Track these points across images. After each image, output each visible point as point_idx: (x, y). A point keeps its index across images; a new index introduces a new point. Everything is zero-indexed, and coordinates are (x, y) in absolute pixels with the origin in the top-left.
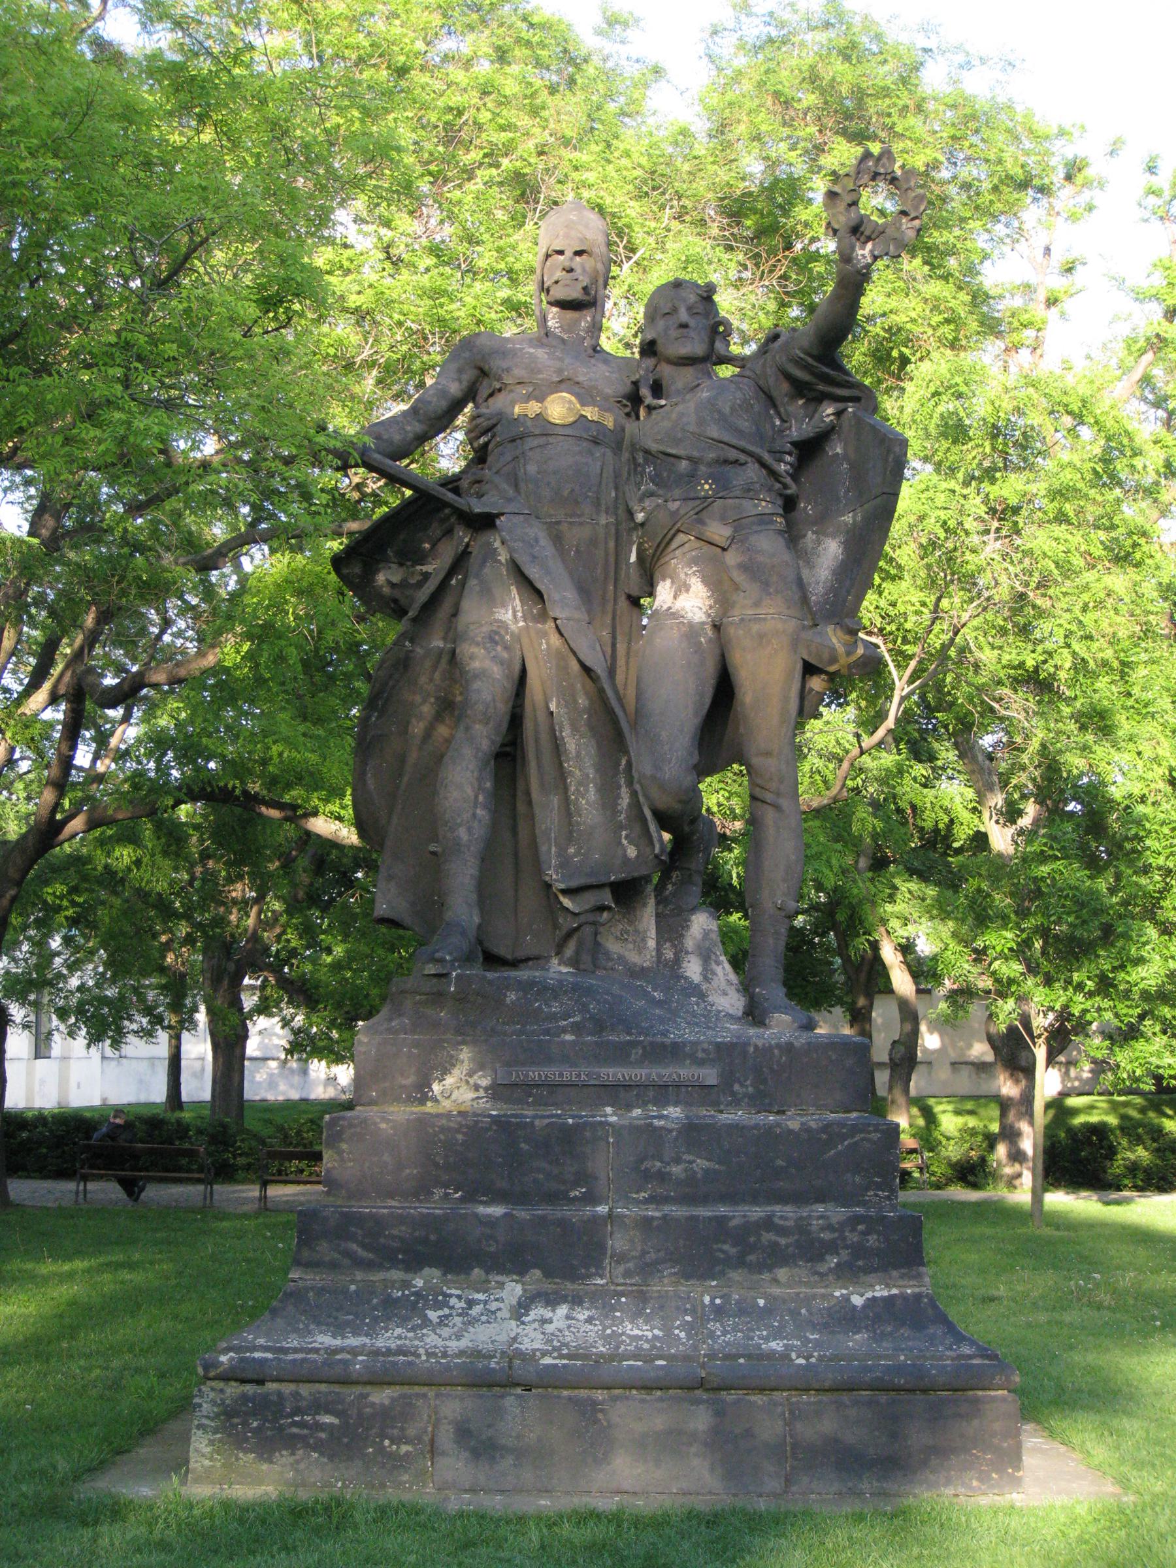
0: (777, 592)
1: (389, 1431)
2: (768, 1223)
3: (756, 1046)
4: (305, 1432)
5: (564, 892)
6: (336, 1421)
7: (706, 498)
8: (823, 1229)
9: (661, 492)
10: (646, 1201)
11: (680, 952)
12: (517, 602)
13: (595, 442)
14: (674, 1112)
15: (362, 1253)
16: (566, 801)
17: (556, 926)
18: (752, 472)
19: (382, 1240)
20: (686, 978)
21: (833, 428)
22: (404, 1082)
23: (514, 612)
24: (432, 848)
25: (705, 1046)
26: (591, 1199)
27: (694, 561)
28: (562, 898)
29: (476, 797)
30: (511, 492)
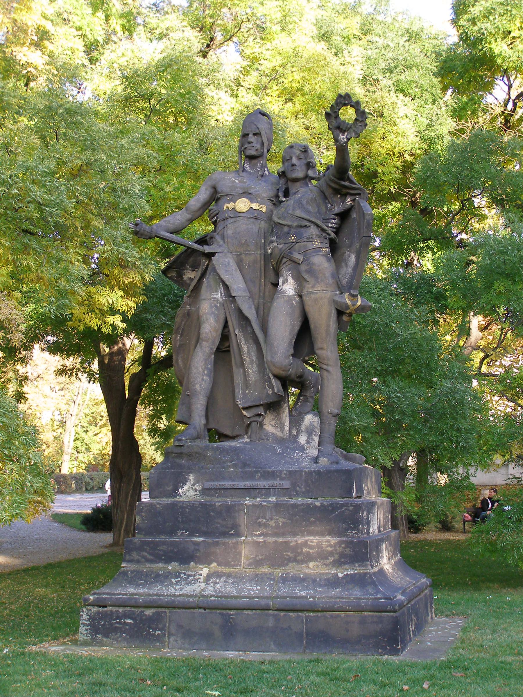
0: (322, 281)
1: (152, 626)
2: (305, 544)
3: (305, 472)
4: (121, 626)
5: (244, 409)
6: (132, 622)
8: (327, 546)
10: (259, 535)
13: (256, 218)
15: (148, 556)
16: (244, 371)
17: (244, 422)
18: (313, 230)
19: (157, 551)
21: (352, 206)
23: (221, 294)
24: (187, 393)
25: (285, 472)
27: (290, 269)
29: (204, 372)
30: (221, 242)
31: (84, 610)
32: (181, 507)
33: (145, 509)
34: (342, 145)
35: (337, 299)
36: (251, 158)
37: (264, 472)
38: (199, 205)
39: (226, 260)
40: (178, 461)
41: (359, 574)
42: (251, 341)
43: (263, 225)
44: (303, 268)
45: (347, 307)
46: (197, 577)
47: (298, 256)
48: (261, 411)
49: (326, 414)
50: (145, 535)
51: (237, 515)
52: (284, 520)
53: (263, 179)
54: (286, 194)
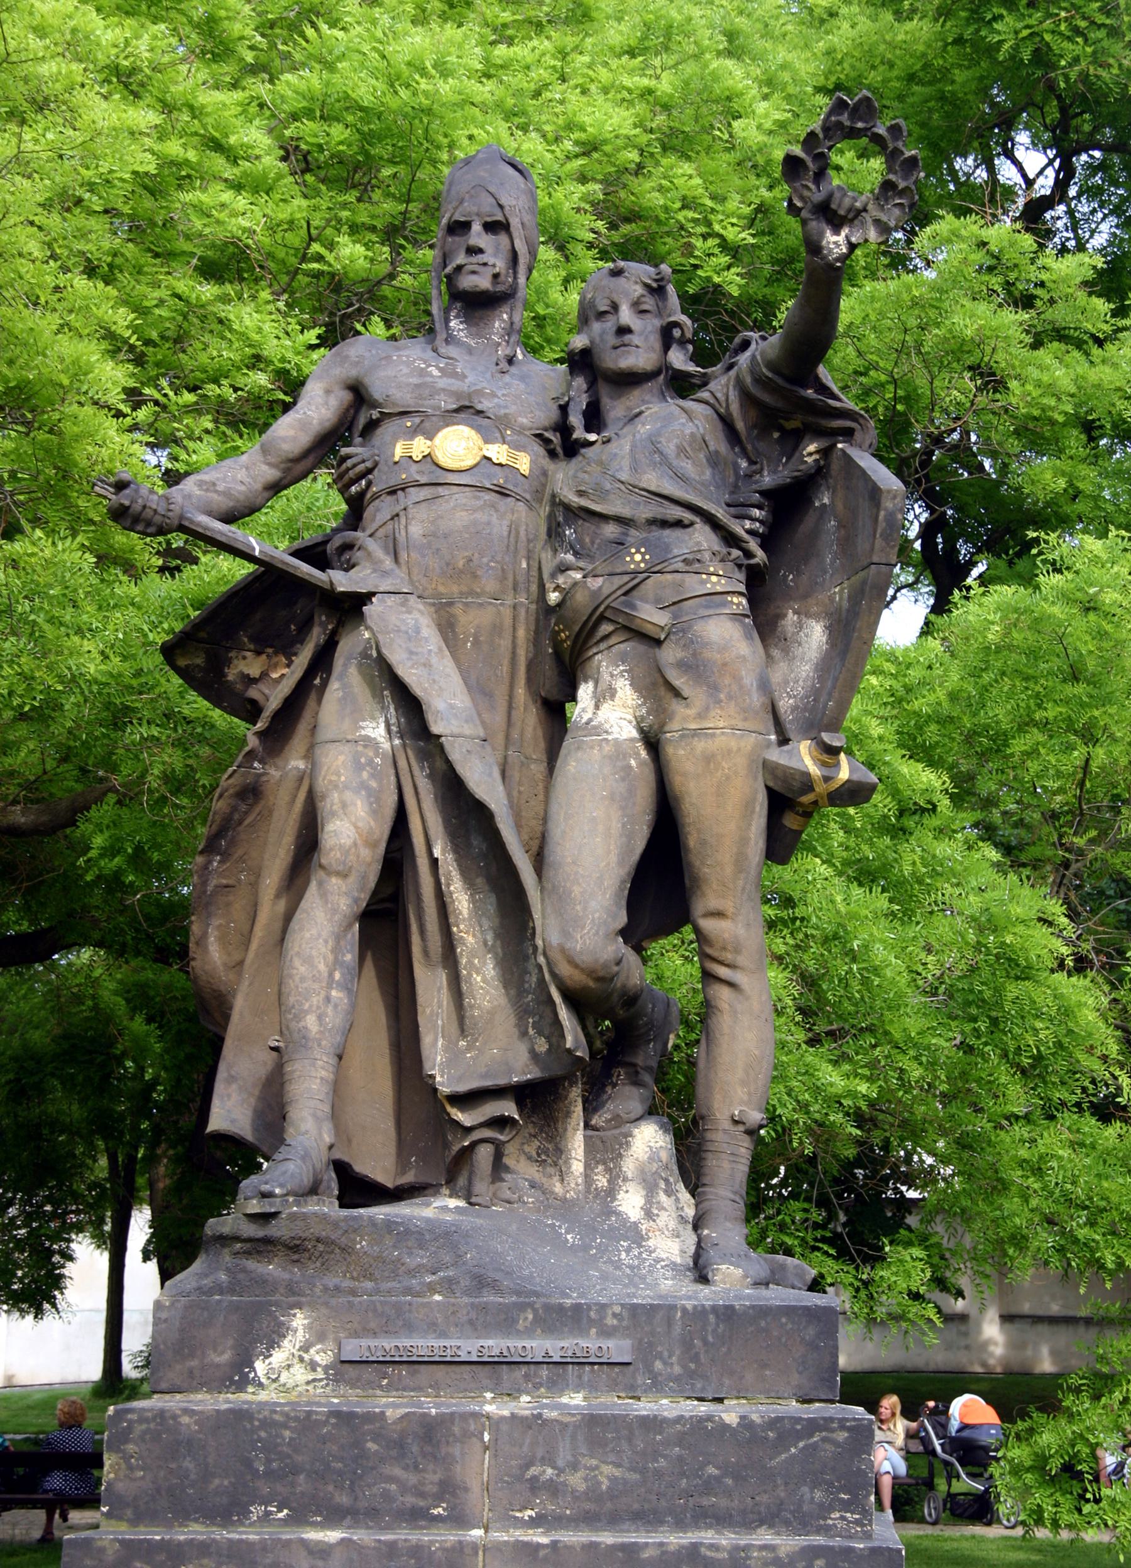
0: (730, 697)
3: (684, 1310)
7: (636, 573)
9: (581, 564)
11: (616, 1177)
12: (392, 710)
13: (502, 493)
14: (575, 1399)
18: (702, 537)
20: (618, 1214)
22: (217, 1360)
25: (617, 1309)
26: (459, 1519)
28: (449, 1109)
29: (331, 975)
30: (388, 563)
32: (266, 1424)
33: (139, 1428)
34: (830, 266)
35: (777, 756)
37: (547, 1307)
38: (304, 440)
39: (410, 619)
42: (480, 881)
45: (807, 783)
47: (652, 616)
48: (508, 1108)
51: (456, 1450)
52: (617, 1472)
53: (513, 370)
54: (594, 418)
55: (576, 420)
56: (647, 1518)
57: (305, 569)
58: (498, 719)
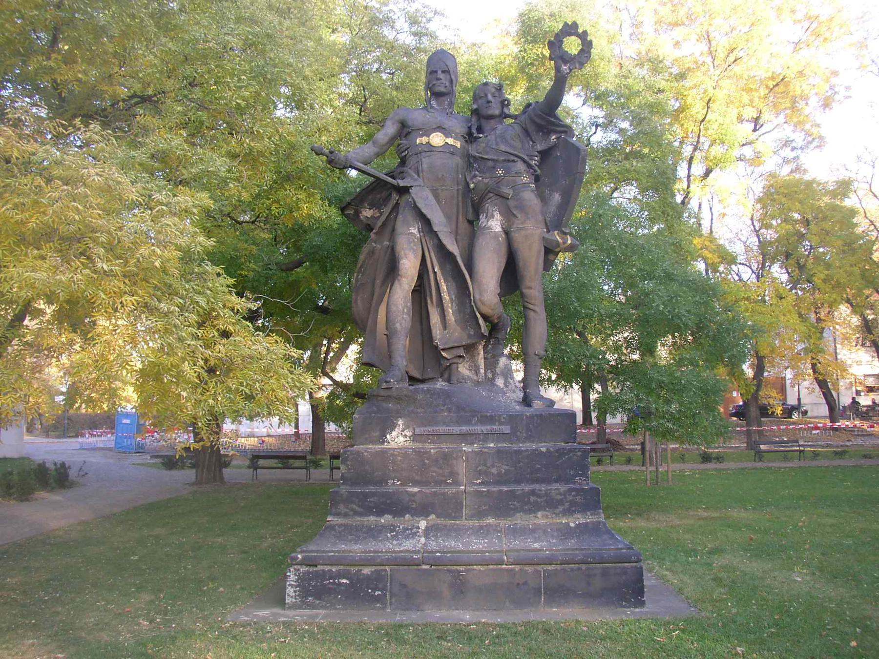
11: (495, 374)
13: (452, 154)
17: (440, 364)
18: (520, 166)
30: (416, 176)
31: (292, 569)
32: (392, 455)
35: (547, 236)
36: (437, 95)
37: (482, 416)
38: (386, 139)
39: (424, 193)
40: (384, 405)
41: (592, 523)
42: (450, 279)
43: (458, 160)
44: (511, 203)
46: (414, 530)
47: (507, 191)
49: (532, 355)
50: (351, 486)
52: (507, 468)
55: (474, 131)
56: (518, 482)
57: (389, 179)
58: (454, 226)
